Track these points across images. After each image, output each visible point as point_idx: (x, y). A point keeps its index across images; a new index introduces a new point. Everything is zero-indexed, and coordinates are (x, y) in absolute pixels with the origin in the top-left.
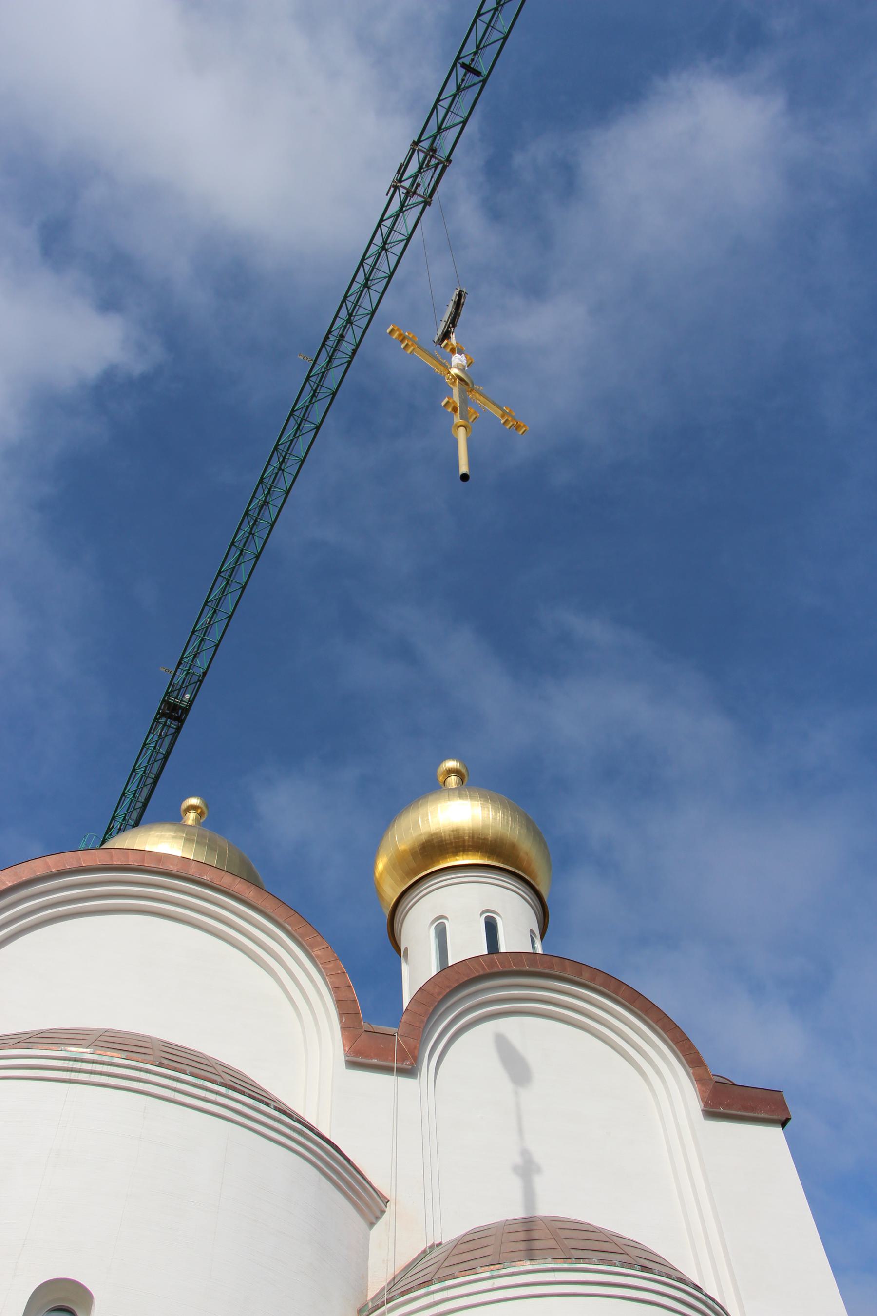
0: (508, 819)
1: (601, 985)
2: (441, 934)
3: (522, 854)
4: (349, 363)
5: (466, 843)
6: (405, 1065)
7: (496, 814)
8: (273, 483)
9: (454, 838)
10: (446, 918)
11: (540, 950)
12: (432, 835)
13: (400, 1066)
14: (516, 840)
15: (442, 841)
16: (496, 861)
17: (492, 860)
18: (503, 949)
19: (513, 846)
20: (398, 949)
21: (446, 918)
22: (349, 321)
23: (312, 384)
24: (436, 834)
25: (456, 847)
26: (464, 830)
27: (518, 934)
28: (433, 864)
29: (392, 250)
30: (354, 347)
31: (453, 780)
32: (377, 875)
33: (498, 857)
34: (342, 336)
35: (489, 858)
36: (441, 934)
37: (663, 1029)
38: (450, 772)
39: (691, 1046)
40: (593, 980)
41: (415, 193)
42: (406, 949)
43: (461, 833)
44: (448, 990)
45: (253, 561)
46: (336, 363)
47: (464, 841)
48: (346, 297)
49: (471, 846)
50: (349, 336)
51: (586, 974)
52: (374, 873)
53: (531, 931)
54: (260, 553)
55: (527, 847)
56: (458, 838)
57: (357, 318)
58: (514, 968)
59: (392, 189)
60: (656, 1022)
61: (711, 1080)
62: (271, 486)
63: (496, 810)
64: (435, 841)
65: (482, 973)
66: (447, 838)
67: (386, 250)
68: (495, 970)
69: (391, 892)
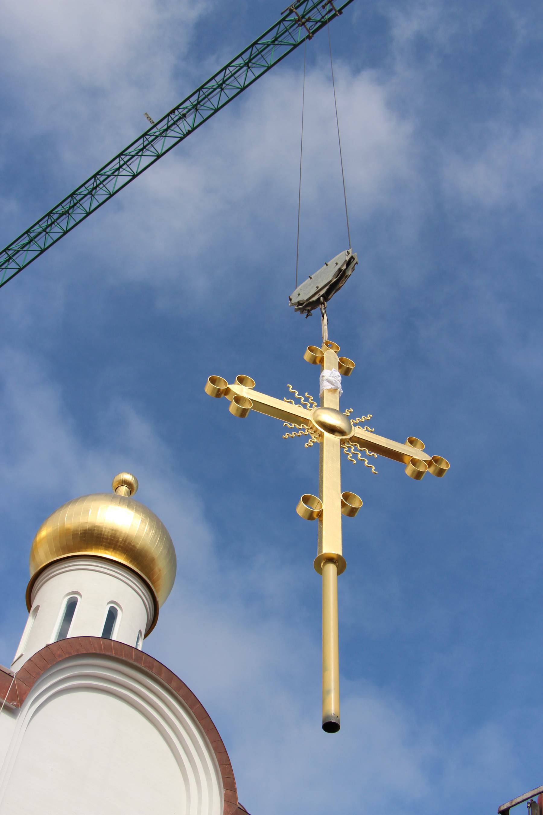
0: (157, 538)
1: (182, 697)
2: (71, 607)
3: (156, 569)
4: (181, 139)
5: (119, 544)
6: (11, 705)
7: (150, 531)
8: (58, 219)
9: (111, 536)
10: (81, 595)
11: (140, 648)
12: (95, 527)
13: (8, 704)
14: (156, 557)
15: (101, 534)
16: (135, 566)
17: (133, 564)
18: (115, 636)
19: (153, 560)
20: (29, 605)
21: (81, 595)
22: (195, 107)
23: (170, 119)
24: (98, 527)
25: (109, 543)
26: (121, 533)
27: (126, 632)
28: (86, 549)
29: (253, 69)
30: (190, 129)
31: (124, 490)
32: (38, 539)
33: (139, 565)
34: (184, 115)
35: (131, 562)
36: (71, 607)
37: (215, 749)
38: (124, 482)
39: (231, 772)
40: (178, 690)
41: (303, 24)
42: (38, 608)
43: (118, 534)
44: (67, 656)
45: (154, 158)
46: (170, 133)
47: (118, 541)
48: (202, 87)
49: (122, 547)
50: (190, 119)
51: (174, 684)
52: (36, 536)
53: (140, 631)
54: (45, 250)
55: (161, 565)
56: (114, 537)
57: (202, 108)
58: (123, 658)
59: (288, 12)
60: (212, 743)
61: (236, 805)
62: (77, 203)
63: (151, 527)
64: (95, 532)
65: (98, 652)
66: (106, 533)
67: (197, 110)
68: (109, 653)
69: (43, 557)
